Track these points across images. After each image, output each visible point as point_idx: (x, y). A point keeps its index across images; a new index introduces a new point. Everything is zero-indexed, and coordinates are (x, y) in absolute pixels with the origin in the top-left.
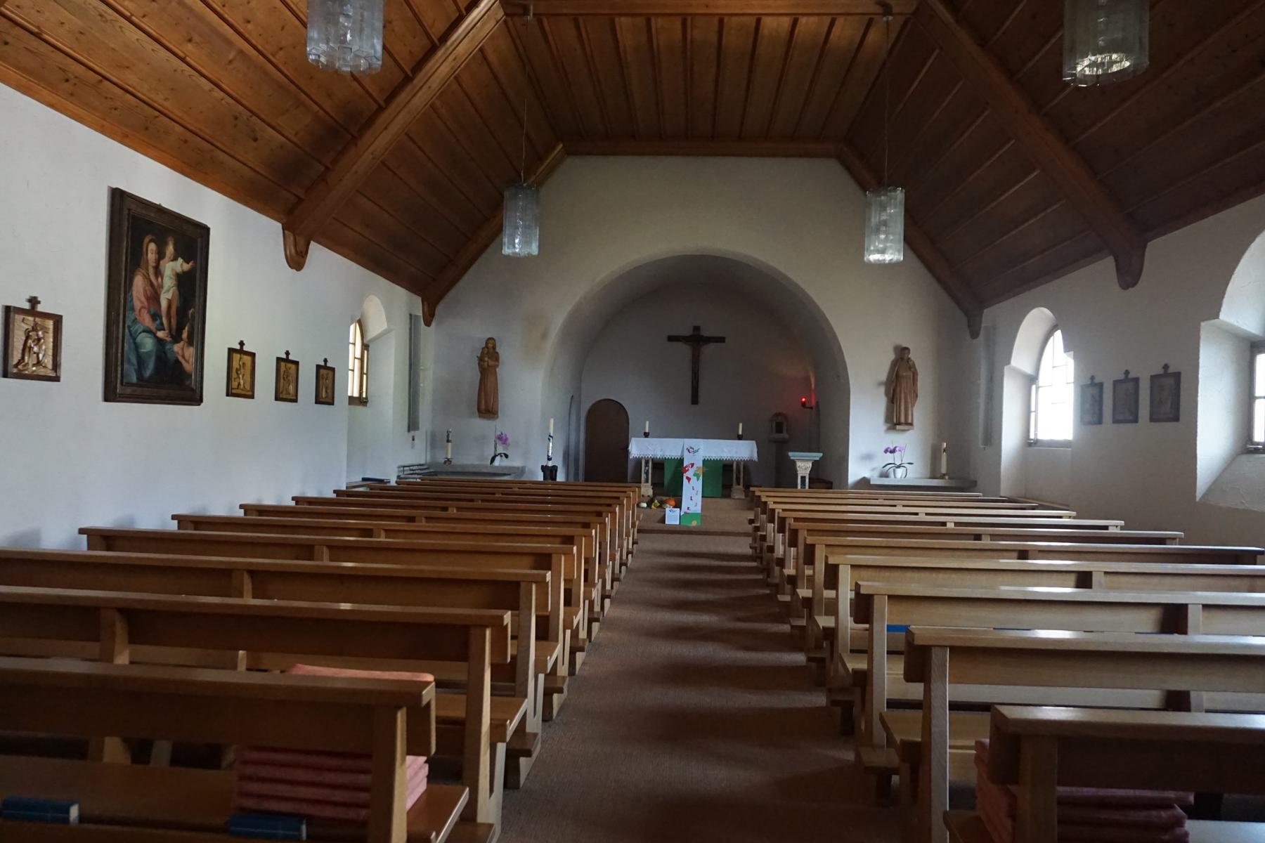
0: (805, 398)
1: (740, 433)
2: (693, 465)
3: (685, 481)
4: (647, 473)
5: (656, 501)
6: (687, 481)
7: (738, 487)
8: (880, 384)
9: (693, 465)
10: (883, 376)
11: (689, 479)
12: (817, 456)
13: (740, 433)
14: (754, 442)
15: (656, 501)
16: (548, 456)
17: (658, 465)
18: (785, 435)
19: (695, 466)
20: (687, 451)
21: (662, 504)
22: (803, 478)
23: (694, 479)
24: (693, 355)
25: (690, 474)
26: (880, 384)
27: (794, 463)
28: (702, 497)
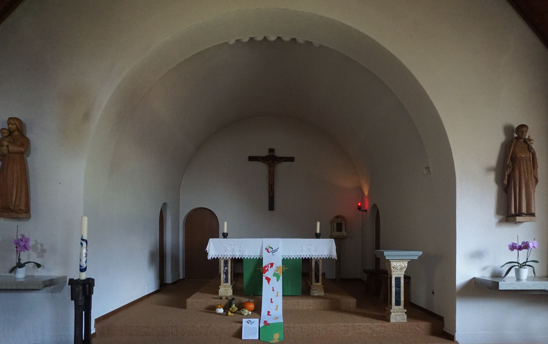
0: (360, 203)
1: (318, 231)
2: (272, 265)
3: (265, 281)
4: (226, 273)
5: (234, 306)
6: (266, 281)
7: (317, 284)
8: (489, 170)
9: (272, 265)
10: (493, 161)
11: (268, 280)
12: (415, 255)
13: (318, 231)
14: (333, 239)
15: (234, 306)
16: (81, 266)
17: (237, 262)
18: (344, 233)
19: (274, 266)
20: (266, 251)
21: (241, 306)
22: (398, 279)
23: (273, 279)
24: (269, 172)
25: (269, 274)
26: (489, 170)
27: (389, 262)
28: (283, 296)
